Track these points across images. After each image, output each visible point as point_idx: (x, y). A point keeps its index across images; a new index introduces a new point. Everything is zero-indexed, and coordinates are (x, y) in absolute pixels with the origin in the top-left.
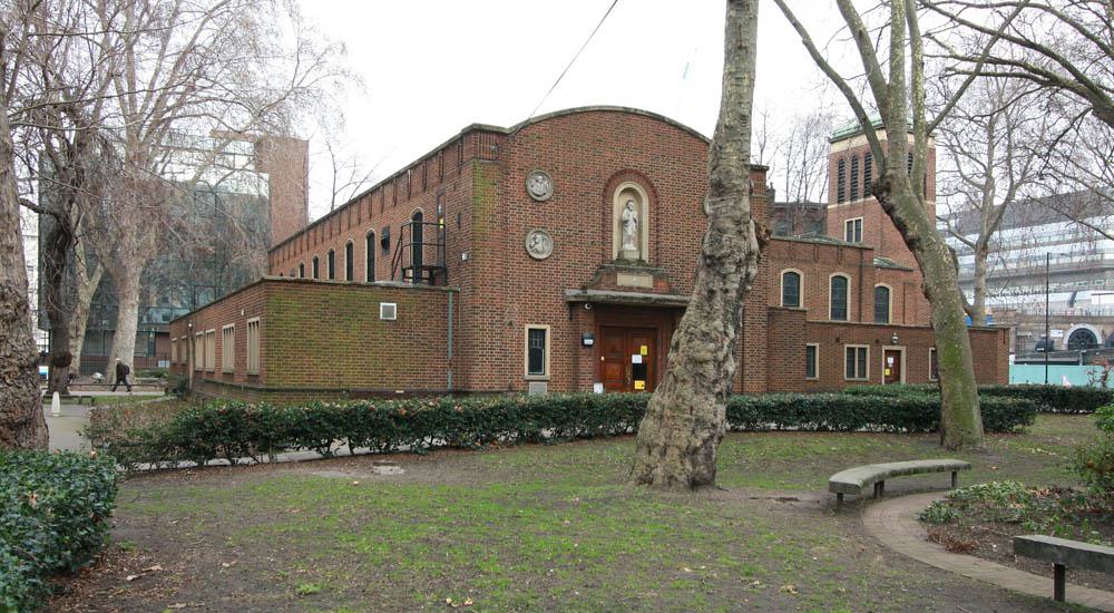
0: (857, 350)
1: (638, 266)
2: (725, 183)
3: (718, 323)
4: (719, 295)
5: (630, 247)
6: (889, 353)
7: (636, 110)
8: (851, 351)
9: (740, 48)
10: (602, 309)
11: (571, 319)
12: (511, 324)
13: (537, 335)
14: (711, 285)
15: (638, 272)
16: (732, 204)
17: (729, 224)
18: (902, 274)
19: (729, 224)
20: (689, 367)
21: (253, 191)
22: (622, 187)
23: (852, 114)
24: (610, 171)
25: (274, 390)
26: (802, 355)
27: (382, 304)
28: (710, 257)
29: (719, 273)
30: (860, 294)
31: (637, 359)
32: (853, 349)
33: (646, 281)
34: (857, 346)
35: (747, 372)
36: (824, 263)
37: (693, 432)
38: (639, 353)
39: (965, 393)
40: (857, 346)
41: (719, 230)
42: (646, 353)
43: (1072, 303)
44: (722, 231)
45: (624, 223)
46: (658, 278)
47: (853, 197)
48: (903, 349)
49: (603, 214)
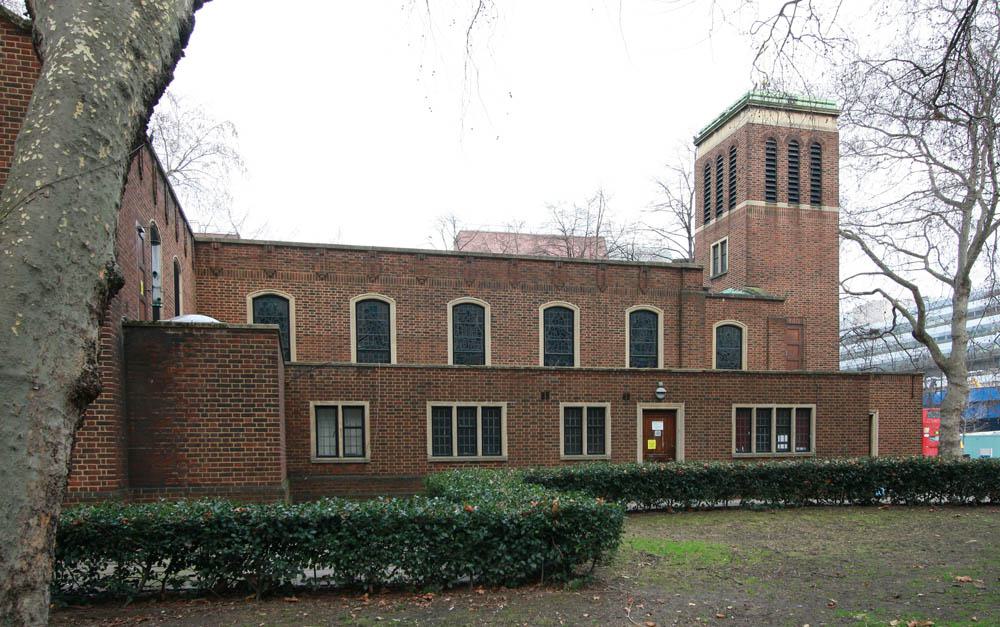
0: (774, 411)
6: (650, 415)
18: (765, 306)
30: (680, 335)
34: (585, 405)
36: (616, 292)
47: (719, 214)
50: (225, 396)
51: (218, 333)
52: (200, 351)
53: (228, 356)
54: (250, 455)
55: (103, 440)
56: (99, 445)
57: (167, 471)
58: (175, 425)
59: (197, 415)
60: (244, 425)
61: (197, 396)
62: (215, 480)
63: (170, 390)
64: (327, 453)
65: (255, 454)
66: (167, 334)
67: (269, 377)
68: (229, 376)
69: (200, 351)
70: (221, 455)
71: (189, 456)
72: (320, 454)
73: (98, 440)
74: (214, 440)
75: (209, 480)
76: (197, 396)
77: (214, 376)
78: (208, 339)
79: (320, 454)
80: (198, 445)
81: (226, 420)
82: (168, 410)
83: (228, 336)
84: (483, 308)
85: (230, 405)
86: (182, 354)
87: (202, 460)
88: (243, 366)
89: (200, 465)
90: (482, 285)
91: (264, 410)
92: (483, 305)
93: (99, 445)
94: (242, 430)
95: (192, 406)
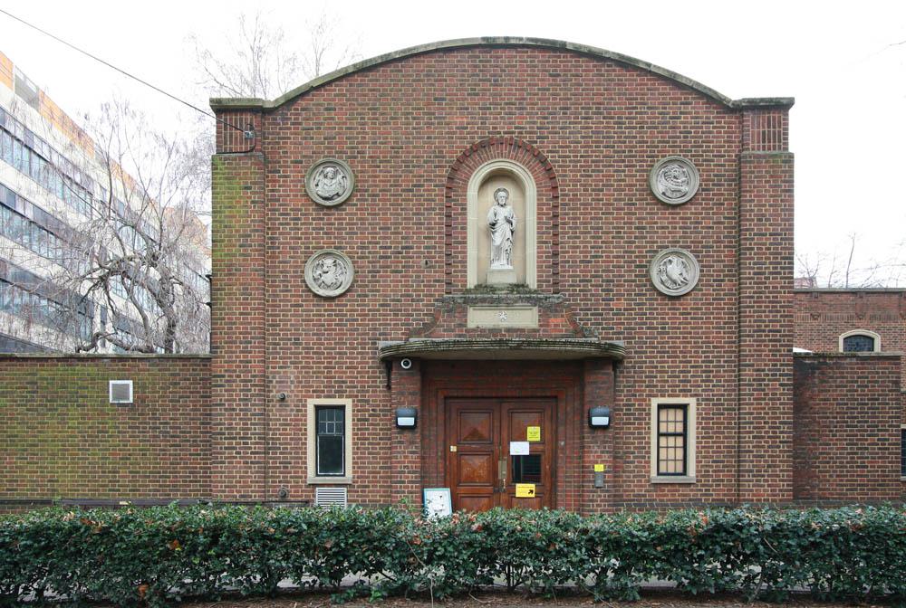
1: (519, 292)
7: (507, 39)
11: (389, 387)
12: (283, 399)
15: (509, 304)
23: (661, 413)
27: (111, 382)
31: (519, 448)
38: (523, 438)
42: (537, 438)
46: (547, 310)
48: (692, 402)
49: (448, 216)
50: (853, 418)
51: (848, 361)
52: (832, 377)
53: (857, 382)
54: (873, 471)
55: (783, 457)
56: (780, 461)
57: (801, 485)
58: (809, 444)
59: (828, 436)
60: (869, 444)
61: (828, 418)
62: (841, 494)
63: (806, 413)
64: (671, 470)
65: (877, 471)
66: (806, 364)
67: (892, 400)
68: (857, 400)
69: (832, 377)
70: (847, 471)
71: (820, 472)
72: (661, 471)
73: (779, 457)
74: (841, 458)
75: (837, 494)
76: (828, 418)
77: (843, 399)
78: (839, 367)
79: (661, 471)
80: (828, 463)
81: (853, 440)
82: (804, 431)
83: (858, 364)
84: (873, 339)
85: (856, 426)
86: (816, 381)
87: (831, 476)
88: (869, 391)
89: (829, 481)
90: (873, 318)
91: (887, 431)
92: (873, 336)
93: (780, 461)
94: (867, 449)
95: (824, 426)
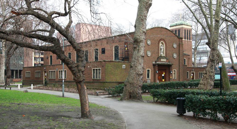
2: (215, 49)
3: (213, 70)
4: (214, 66)
5: (162, 54)
8: (200, 73)
9: (218, 28)
10: (159, 65)
13: (148, 71)
14: (212, 64)
16: (216, 52)
17: (215, 55)
18: (188, 56)
19: (215, 55)
20: (209, 77)
21: (42, 34)
22: (161, 42)
24: (159, 39)
25: (107, 82)
26: (186, 74)
27: (123, 65)
28: (212, 60)
29: (214, 62)
31: (163, 75)
32: (60, 71)
33: (165, 60)
35: (180, 77)
37: (210, 87)
38: (163, 74)
39: (227, 80)
40: (98, 68)
41: (213, 56)
43: (200, 60)
44: (214, 56)
45: (161, 49)
46: (167, 60)
